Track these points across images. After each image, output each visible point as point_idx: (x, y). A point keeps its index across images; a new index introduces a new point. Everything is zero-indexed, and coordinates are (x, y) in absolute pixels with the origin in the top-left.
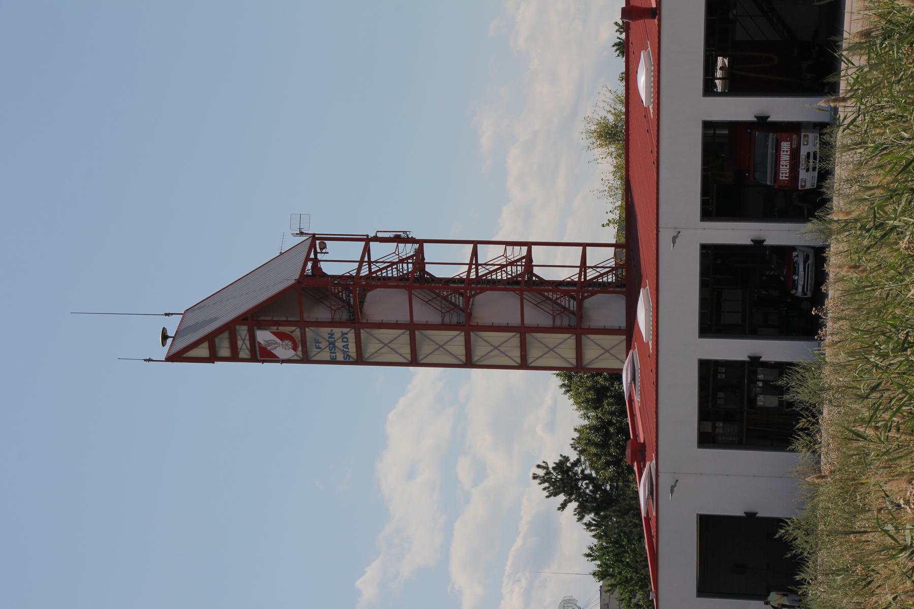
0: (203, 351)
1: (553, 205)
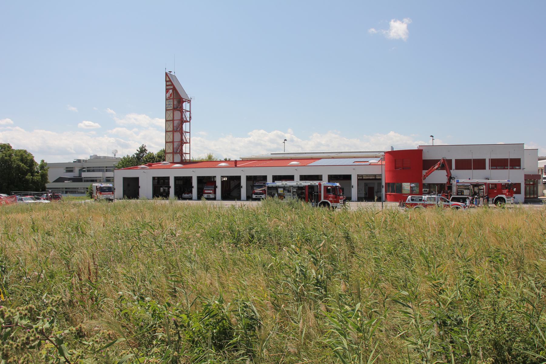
0: (168, 79)
1: (197, 147)
